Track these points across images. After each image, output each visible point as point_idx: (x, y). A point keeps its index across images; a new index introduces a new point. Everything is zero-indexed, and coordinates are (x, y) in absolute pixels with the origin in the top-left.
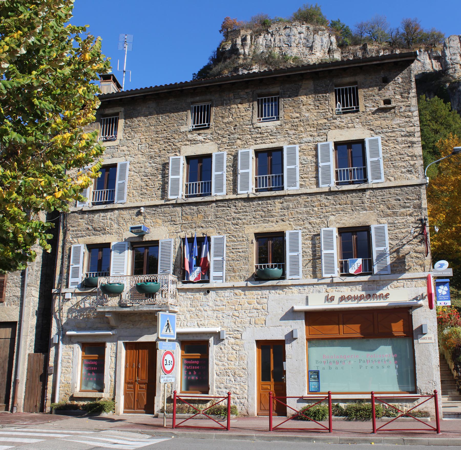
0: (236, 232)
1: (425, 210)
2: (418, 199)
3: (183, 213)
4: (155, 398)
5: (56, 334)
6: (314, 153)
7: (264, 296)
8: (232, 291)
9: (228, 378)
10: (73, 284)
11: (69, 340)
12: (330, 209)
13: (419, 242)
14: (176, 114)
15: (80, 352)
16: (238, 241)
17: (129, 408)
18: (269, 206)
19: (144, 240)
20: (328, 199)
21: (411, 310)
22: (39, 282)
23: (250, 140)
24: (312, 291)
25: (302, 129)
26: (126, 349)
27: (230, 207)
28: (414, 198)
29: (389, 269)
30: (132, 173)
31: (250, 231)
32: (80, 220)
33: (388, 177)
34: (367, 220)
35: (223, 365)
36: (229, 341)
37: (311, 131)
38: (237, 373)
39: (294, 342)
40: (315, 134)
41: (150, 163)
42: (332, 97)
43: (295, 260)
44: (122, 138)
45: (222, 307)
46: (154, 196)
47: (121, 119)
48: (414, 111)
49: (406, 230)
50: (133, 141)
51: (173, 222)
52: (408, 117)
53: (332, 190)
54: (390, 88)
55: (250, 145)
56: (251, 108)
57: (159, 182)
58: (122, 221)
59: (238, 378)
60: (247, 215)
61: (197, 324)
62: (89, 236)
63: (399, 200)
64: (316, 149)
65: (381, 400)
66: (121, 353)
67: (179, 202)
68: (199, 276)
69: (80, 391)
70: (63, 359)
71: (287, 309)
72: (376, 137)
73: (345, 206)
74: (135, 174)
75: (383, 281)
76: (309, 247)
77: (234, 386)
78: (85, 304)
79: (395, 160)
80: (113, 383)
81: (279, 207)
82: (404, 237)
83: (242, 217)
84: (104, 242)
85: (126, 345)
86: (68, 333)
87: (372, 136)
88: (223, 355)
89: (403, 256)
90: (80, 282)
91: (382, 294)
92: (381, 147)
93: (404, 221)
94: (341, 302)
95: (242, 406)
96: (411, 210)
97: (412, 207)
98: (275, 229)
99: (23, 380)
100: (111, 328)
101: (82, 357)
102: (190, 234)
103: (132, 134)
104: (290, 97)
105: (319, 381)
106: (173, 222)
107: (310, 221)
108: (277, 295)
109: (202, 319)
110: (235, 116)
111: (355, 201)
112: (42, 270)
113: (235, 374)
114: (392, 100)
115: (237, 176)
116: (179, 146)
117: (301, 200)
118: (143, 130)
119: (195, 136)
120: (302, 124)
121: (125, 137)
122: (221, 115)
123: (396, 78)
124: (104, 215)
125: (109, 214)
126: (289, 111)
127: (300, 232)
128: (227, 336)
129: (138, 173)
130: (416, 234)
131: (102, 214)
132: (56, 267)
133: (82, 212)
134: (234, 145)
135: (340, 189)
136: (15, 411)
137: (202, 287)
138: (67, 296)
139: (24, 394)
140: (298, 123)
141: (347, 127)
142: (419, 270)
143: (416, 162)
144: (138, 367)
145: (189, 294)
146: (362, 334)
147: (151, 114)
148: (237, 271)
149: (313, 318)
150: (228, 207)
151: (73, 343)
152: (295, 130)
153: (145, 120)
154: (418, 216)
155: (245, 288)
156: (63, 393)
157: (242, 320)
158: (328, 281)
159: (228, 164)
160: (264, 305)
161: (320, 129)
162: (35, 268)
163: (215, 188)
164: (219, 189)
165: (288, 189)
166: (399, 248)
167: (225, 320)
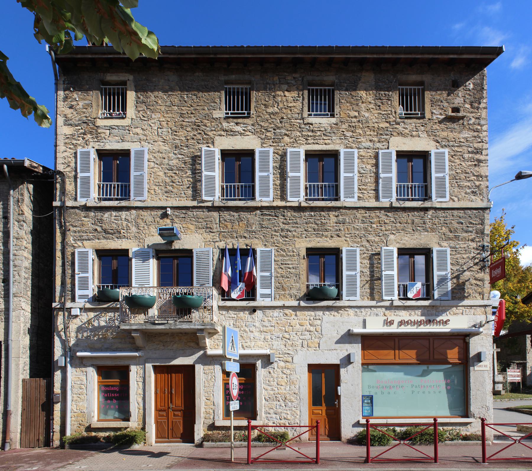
0: (285, 245)
1: (487, 236)
2: (481, 224)
3: (221, 219)
4: (195, 426)
5: (62, 356)
6: (374, 161)
7: (318, 317)
8: (281, 311)
9: (278, 403)
10: (81, 297)
11: (81, 363)
12: (390, 227)
13: (480, 269)
14: (206, 94)
15: (96, 376)
16: (287, 255)
17: (162, 438)
18: (323, 218)
19: (173, 248)
20: (388, 216)
21: (468, 338)
22: (29, 293)
23: (300, 138)
24: (369, 313)
25: (361, 132)
26: (155, 373)
27: (278, 217)
28: (477, 223)
29: (450, 294)
30: (152, 164)
31: (302, 245)
32: (83, 219)
33: (452, 197)
34: (429, 243)
35: (273, 390)
36: (278, 364)
37: (371, 135)
38: (288, 398)
39: (350, 367)
40: (376, 139)
41: (175, 154)
42: (395, 96)
43: (352, 280)
44: (134, 117)
45: (270, 328)
46: (183, 195)
47: (131, 90)
48: (484, 125)
49: (467, 255)
50: (149, 122)
51: (209, 230)
52: (477, 131)
53: (394, 205)
54: (460, 95)
55: (301, 144)
56: (301, 99)
57: (189, 179)
58: (142, 224)
59: (289, 403)
60: (297, 227)
61: (242, 345)
62: (98, 239)
63: (462, 224)
64: (376, 157)
66: (150, 377)
67: (216, 204)
68: (242, 293)
69: (98, 421)
70: (73, 384)
71: (343, 331)
72: (441, 150)
73: (406, 225)
74: (156, 166)
75: (442, 307)
76: (366, 267)
77: (285, 411)
78: (99, 322)
79: (460, 179)
80: (141, 411)
81: (334, 221)
82: (465, 263)
83: (292, 229)
84: (120, 248)
85: (155, 367)
86: (79, 354)
87: (437, 149)
88: (272, 379)
89: (463, 282)
90: (91, 295)
91: (443, 320)
92: (447, 163)
93: (465, 246)
94: (400, 326)
95: (294, 432)
96: (473, 236)
97: (474, 232)
98: (329, 245)
99: (17, 410)
100: (137, 350)
101: (98, 382)
102: (231, 244)
103: (148, 113)
104: (347, 90)
105: (372, 406)
106: (210, 230)
107: (368, 239)
108: (332, 317)
109: (247, 341)
110: (281, 105)
111: (416, 221)
112: (32, 279)
113: (285, 401)
114: (462, 109)
115: (286, 180)
116: (212, 136)
117: (360, 214)
118: (163, 108)
119: (231, 125)
120: (361, 126)
121: (138, 116)
122: (263, 102)
123: (467, 83)
124: (117, 214)
125: (124, 214)
126: (346, 108)
127: (358, 250)
129: (160, 165)
130: (477, 261)
131: (114, 213)
132: (55, 276)
133: (86, 208)
134: (280, 142)
135: (402, 206)
136: (7, 448)
137: (248, 305)
138: (74, 312)
139: (19, 427)
140: (357, 124)
141: (411, 136)
142: (478, 298)
143: (481, 183)
144: (171, 393)
145: (232, 313)
146: (417, 360)
147: (172, 90)
148: (287, 289)
149: (370, 341)
150: (276, 216)
151: (85, 366)
152: (352, 132)
153: (165, 97)
155: (296, 308)
156: (76, 423)
157: (293, 342)
158: (387, 304)
159: (274, 165)
160: (317, 327)
161: (381, 134)
162: (23, 274)
163: (260, 192)
164: (265, 193)
165: (345, 201)
166: (460, 274)
167: (275, 342)
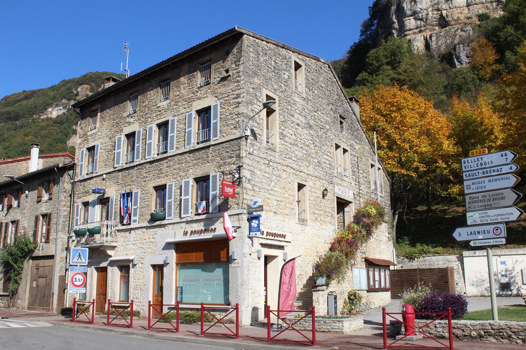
40: (186, 106)
65: (210, 310)
128: (138, 262)
143: (239, 119)
147: (111, 107)
149: (180, 247)
154: (237, 164)
